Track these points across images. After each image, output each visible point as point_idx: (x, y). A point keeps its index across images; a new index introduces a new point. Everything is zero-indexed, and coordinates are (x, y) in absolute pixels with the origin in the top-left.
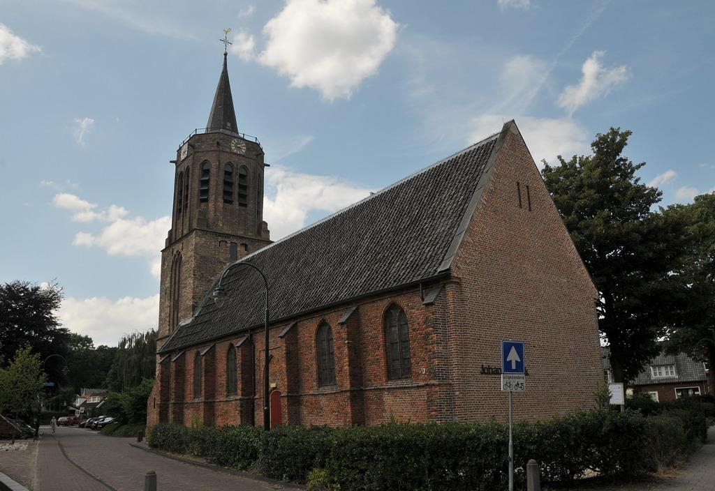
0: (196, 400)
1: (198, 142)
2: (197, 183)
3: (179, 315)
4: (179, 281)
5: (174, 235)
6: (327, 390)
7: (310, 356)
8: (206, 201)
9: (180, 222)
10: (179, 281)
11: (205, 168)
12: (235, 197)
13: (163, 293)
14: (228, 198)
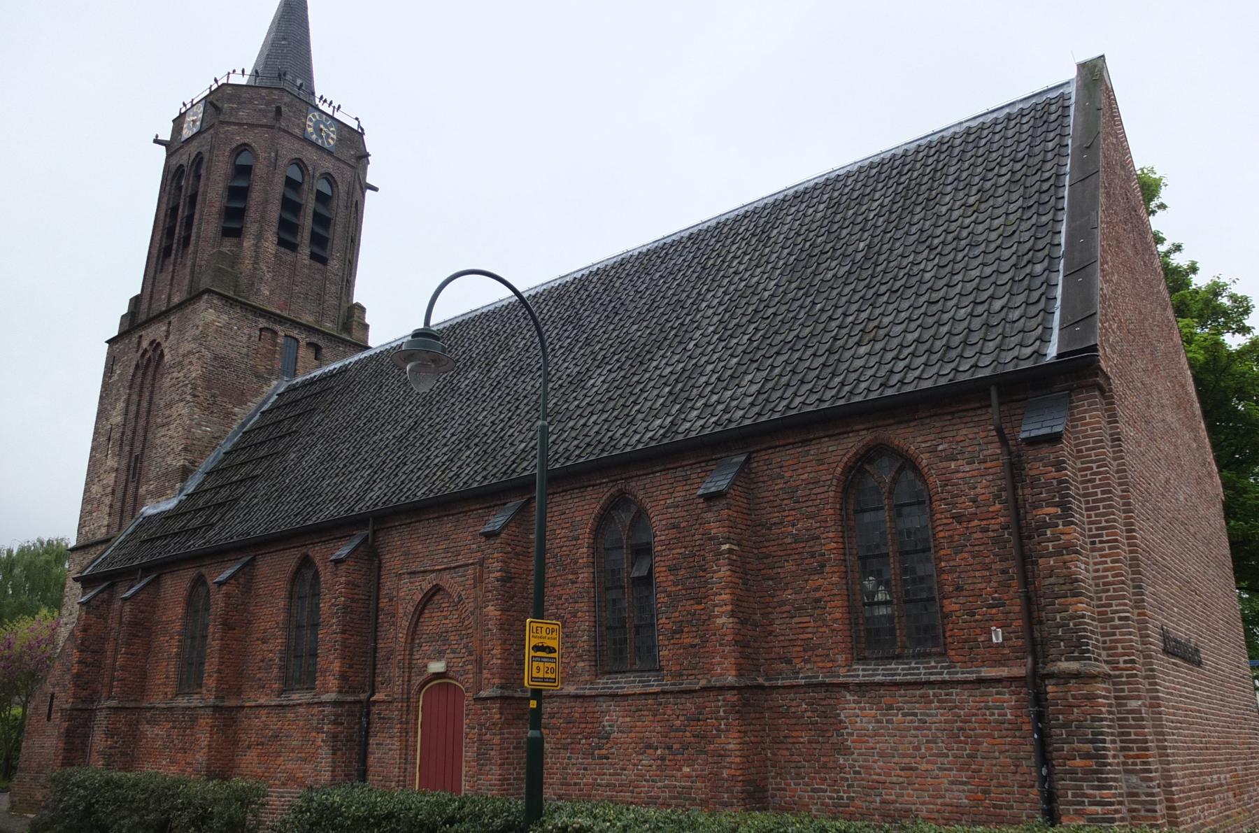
0: (182, 702)
2: (221, 190)
3: (142, 490)
4: (149, 412)
5: (144, 306)
6: (628, 684)
9: (165, 277)
10: (149, 412)
11: (244, 160)
12: (304, 238)
14: (287, 237)
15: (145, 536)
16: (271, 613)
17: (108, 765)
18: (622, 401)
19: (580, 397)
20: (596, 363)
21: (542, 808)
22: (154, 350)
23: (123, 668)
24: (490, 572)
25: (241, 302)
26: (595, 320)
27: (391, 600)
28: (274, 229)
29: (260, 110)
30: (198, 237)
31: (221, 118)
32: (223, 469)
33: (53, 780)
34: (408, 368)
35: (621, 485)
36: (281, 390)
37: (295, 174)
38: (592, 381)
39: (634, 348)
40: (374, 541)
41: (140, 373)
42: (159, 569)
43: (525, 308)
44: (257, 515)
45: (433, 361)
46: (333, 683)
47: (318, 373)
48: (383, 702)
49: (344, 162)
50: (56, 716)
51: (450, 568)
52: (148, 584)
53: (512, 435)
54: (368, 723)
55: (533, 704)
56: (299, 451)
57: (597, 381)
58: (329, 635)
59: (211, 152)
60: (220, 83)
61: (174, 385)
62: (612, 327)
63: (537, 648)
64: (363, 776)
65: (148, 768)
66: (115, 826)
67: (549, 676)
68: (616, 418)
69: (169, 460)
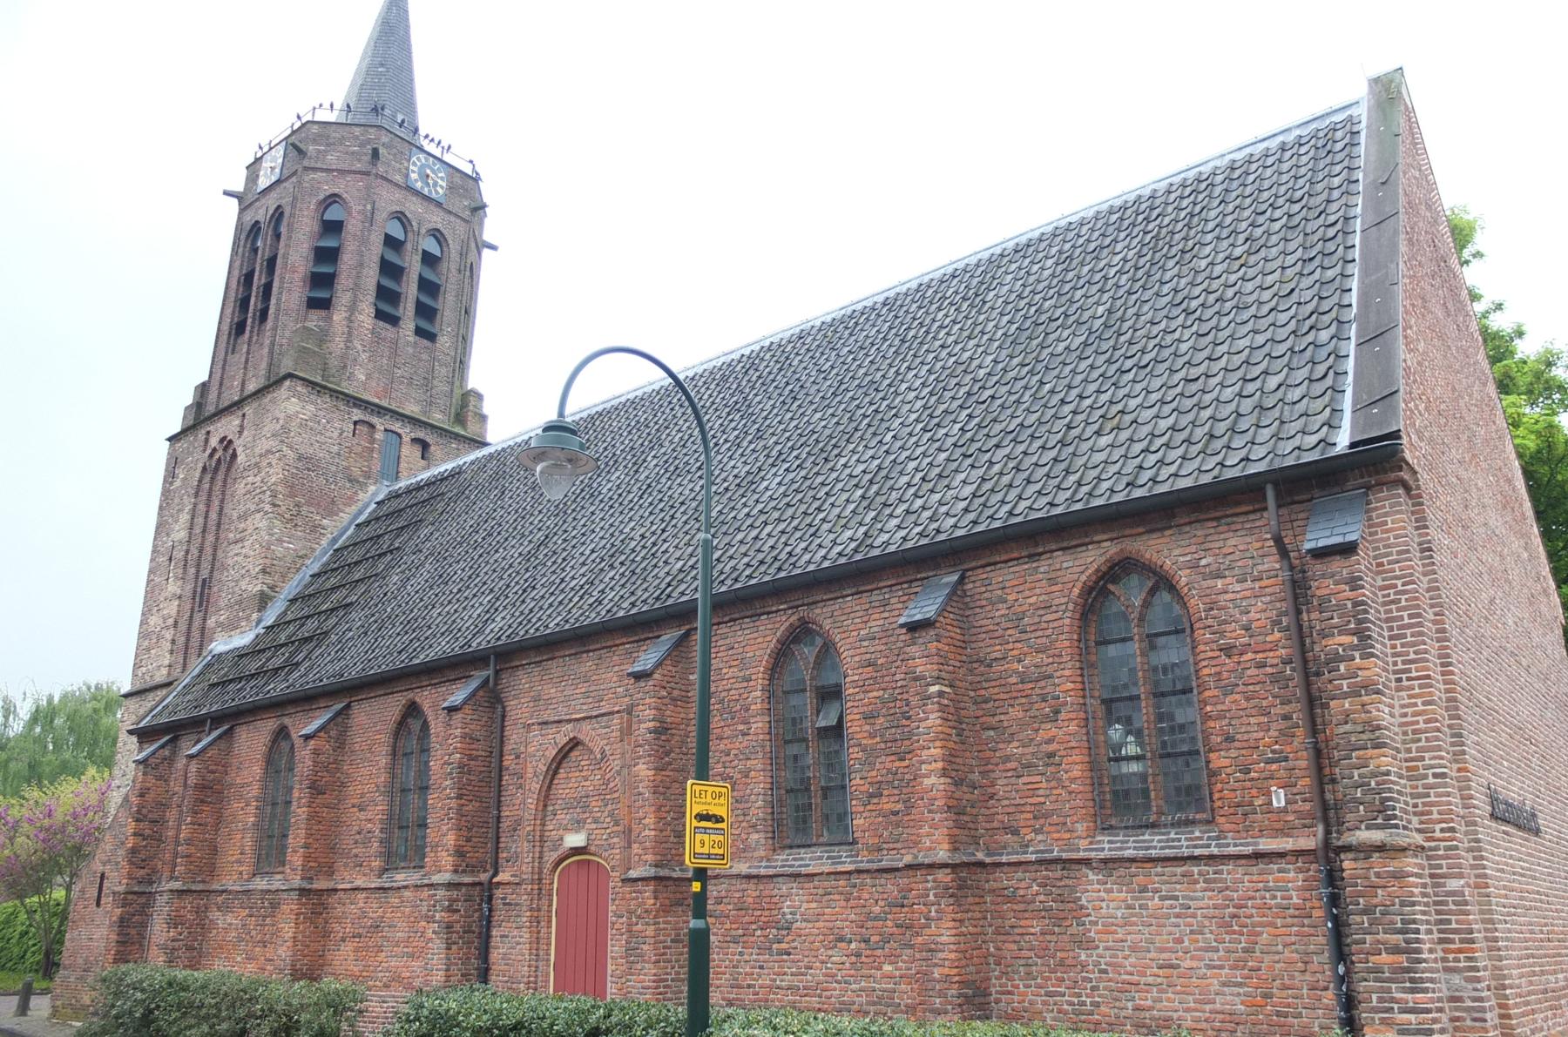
3: (211, 622)
4: (219, 525)
6: (813, 860)
7: (741, 742)
8: (323, 304)
9: (238, 359)
10: (219, 525)
11: (333, 214)
12: (407, 310)
13: (163, 559)
15: (214, 679)
16: (369, 771)
18: (803, 508)
19: (751, 503)
20: (771, 461)
21: (708, 1017)
22: (225, 449)
23: (189, 842)
24: (640, 722)
26: (768, 407)
27: (518, 757)
30: (278, 310)
31: (306, 163)
34: (538, 469)
36: (380, 497)
37: (396, 231)
38: (765, 484)
39: (817, 441)
40: (496, 684)
45: (570, 461)
46: (447, 860)
47: (425, 475)
49: (456, 215)
50: (107, 900)
52: (220, 737)
54: (490, 910)
55: (696, 887)
57: (772, 483)
58: (442, 802)
59: (293, 205)
62: (789, 415)
69: (243, 584)
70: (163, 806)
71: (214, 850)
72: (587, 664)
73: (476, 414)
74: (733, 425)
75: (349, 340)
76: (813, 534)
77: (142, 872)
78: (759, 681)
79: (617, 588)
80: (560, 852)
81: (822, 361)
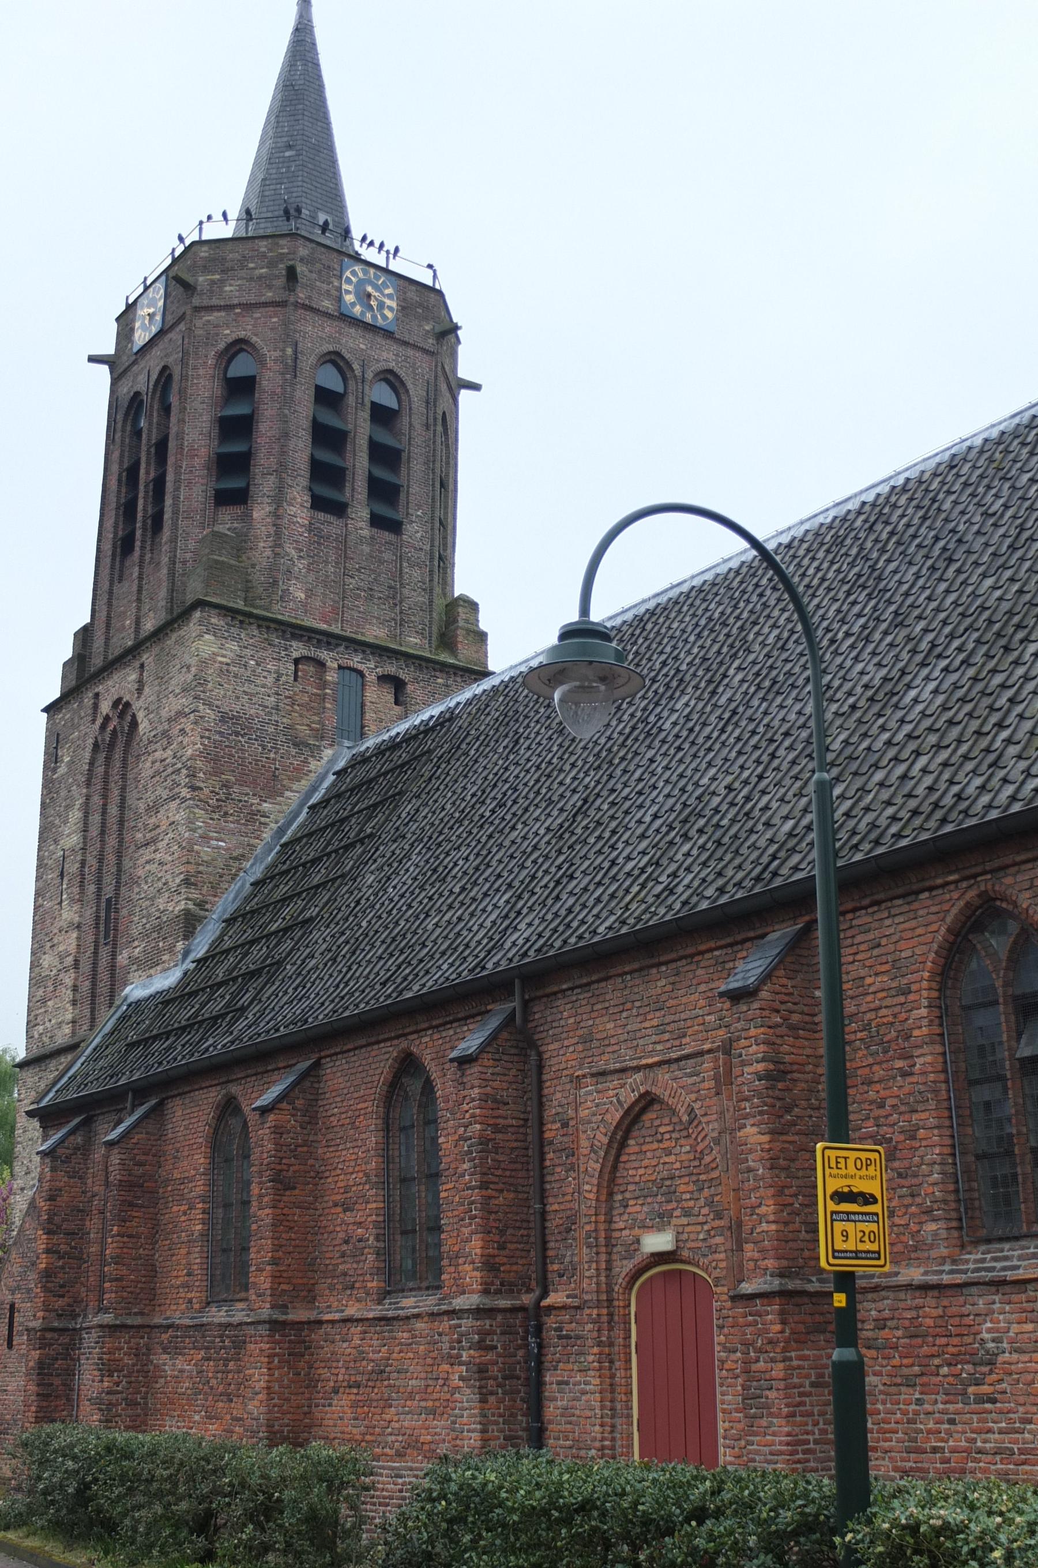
1: (206, 269)
3: (122, 958)
4: (121, 822)
5: (98, 643)
7: (902, 1087)
9: (128, 588)
10: (121, 822)
11: (240, 368)
12: (357, 493)
13: (52, 876)
14: (326, 492)
15: (133, 1036)
16: (355, 1155)
17: (107, 1422)
18: (975, 725)
19: (893, 724)
20: (919, 658)
21: (869, 1492)
23: (118, 1260)
24: (743, 1064)
25: (258, 617)
26: (909, 577)
27: (565, 1125)
28: (304, 481)
29: (260, 277)
30: (176, 512)
31: (196, 301)
32: (253, 912)
33: (25, 1445)
34: (557, 696)
35: (985, 883)
36: (341, 764)
37: (331, 380)
38: (913, 693)
39: (990, 622)
40: (525, 1021)
41: (102, 757)
42: (162, 1089)
43: (770, 568)
44: (314, 990)
45: (603, 679)
46: (472, 1276)
47: (402, 727)
48: (564, 1307)
49: (414, 347)
50: (21, 1340)
51: (669, 1062)
52: (146, 1116)
53: (766, 808)
54: (540, 1346)
55: (840, 1300)
56: (381, 869)
57: (923, 691)
58: (459, 1191)
59: (183, 362)
60: (188, 242)
61: (158, 773)
62: (943, 586)
63: (840, 1197)
64: (538, 1438)
65: (172, 1427)
66: (127, 1522)
67: (868, 1246)
68: (966, 757)
69: (161, 902)
70: (82, 1213)
71: (152, 1271)
72: (659, 983)
73: (469, 631)
74: (856, 609)
75: (277, 544)
76: (994, 764)
77: (61, 1302)
78: (923, 994)
79: (696, 869)
80: (637, 1259)
81: (989, 499)
